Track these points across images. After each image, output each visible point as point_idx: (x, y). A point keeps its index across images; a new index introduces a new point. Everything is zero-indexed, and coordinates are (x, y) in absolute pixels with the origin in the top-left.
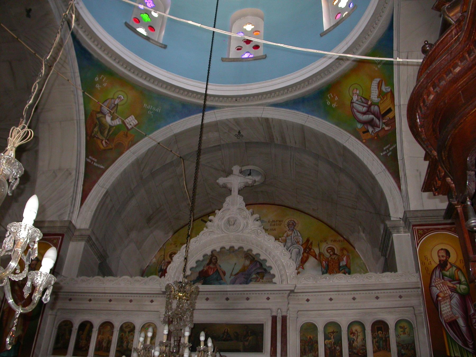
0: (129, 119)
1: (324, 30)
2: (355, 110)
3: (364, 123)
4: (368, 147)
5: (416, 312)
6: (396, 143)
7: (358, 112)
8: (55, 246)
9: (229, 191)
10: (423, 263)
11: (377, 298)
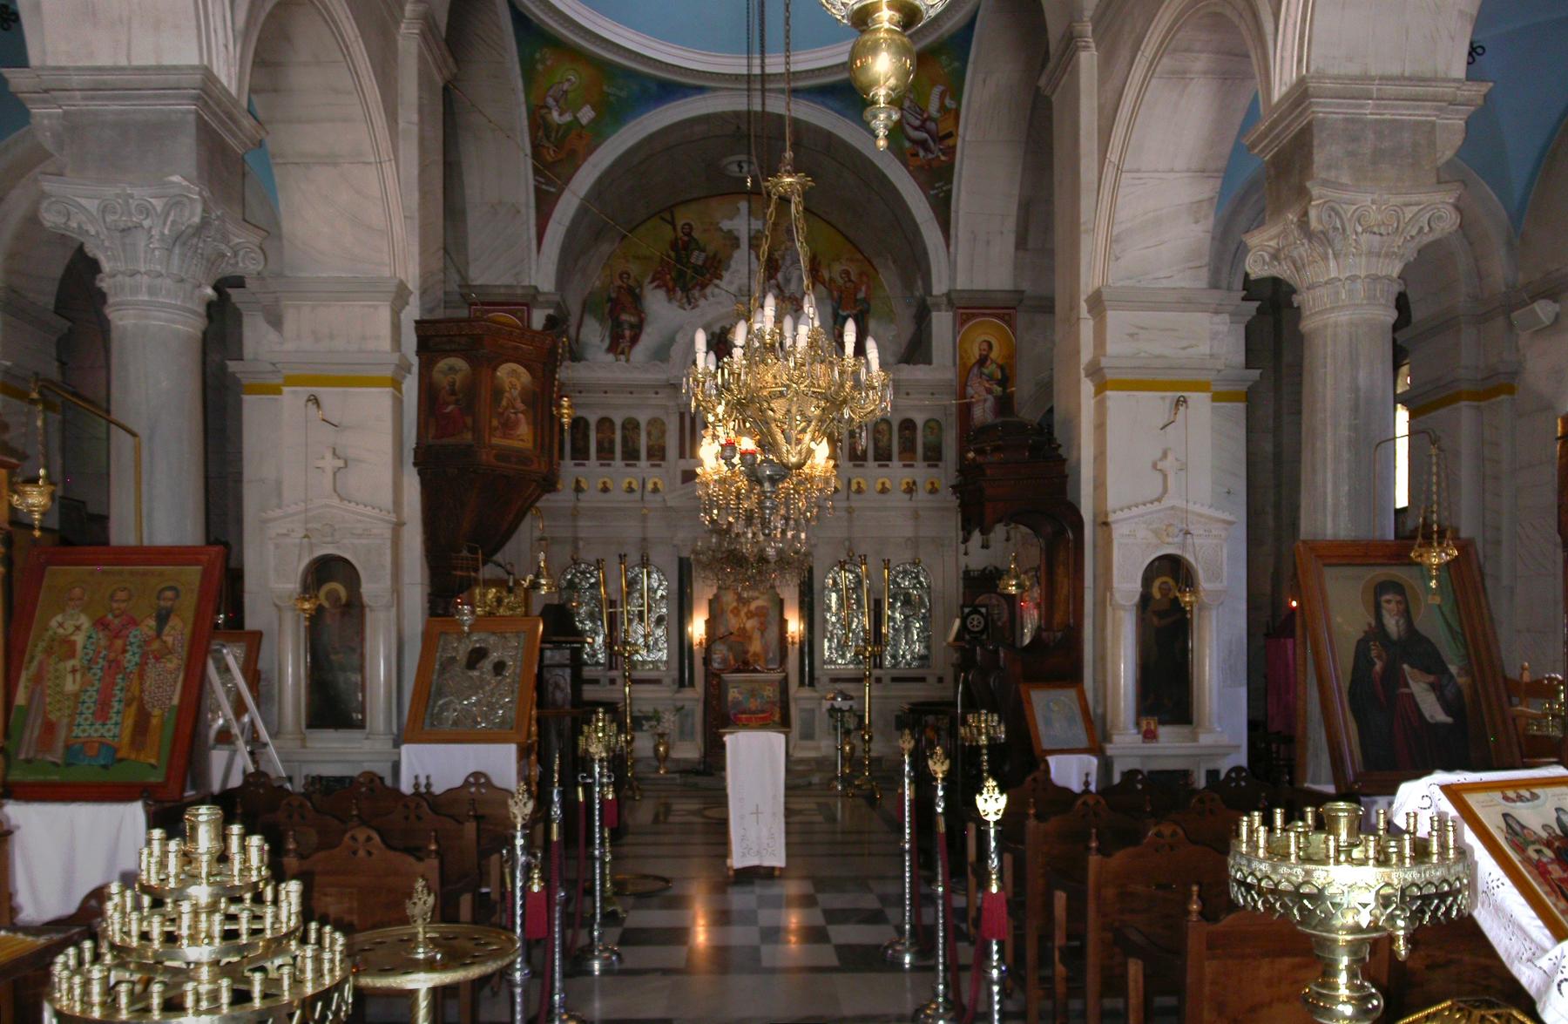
4: (915, 178)
8: (537, 332)
10: (961, 358)
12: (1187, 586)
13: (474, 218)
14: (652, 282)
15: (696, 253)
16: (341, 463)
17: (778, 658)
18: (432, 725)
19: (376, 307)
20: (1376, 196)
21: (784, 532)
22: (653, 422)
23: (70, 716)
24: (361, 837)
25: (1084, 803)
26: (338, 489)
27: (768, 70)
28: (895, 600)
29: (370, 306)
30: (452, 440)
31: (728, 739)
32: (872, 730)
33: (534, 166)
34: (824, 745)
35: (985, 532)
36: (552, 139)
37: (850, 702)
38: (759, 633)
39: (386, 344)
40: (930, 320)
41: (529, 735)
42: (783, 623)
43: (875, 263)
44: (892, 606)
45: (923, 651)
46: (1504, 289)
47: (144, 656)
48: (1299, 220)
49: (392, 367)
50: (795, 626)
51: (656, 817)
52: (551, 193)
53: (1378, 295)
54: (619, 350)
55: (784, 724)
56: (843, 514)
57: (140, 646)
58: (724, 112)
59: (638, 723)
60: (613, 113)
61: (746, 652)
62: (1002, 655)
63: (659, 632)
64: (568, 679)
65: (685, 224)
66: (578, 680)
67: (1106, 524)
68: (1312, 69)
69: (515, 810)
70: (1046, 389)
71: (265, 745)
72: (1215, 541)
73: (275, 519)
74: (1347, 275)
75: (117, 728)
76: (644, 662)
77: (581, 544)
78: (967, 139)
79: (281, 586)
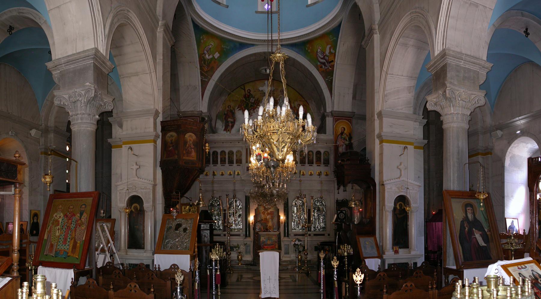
0: (216, 54)
1: (309, 4)
2: (318, 56)
3: (321, 63)
6: (333, 77)
7: (319, 57)
9: (264, 94)
10: (335, 132)
12: (407, 205)
13: (182, 91)
14: (238, 108)
15: (252, 99)
17: (277, 228)
18: (164, 248)
19: (149, 118)
20: (464, 90)
21: (279, 185)
22: (238, 152)
23: (57, 242)
24: (133, 286)
25: (380, 275)
26: (137, 175)
27: (273, 38)
28: (315, 210)
29: (147, 118)
30: (171, 158)
31: (260, 254)
32: (308, 251)
33: (200, 71)
34: (292, 256)
35: (345, 186)
36: (206, 64)
37: (301, 242)
38: (271, 220)
39: (152, 129)
40: (326, 119)
41: (194, 252)
42: (279, 217)
43: (308, 102)
44: (314, 211)
45: (323, 226)
46: (489, 126)
47: (76, 225)
48: (443, 94)
49: (154, 136)
50: (282, 217)
51: (238, 279)
52: (206, 81)
53: (464, 120)
54: (228, 129)
55: (279, 249)
56: (298, 182)
57: (75, 222)
58: (260, 52)
59: (232, 248)
60: (225, 54)
61: (267, 226)
62: (351, 226)
63: (239, 219)
64: (209, 234)
65: (248, 90)
66: (212, 235)
67: (383, 185)
68: (447, 47)
69: (177, 278)
70: (363, 142)
71: (115, 253)
72: (415, 192)
73: (119, 185)
74: (456, 112)
75: (68, 247)
76: (235, 229)
77: (215, 192)
78: (338, 63)
79: (121, 205)
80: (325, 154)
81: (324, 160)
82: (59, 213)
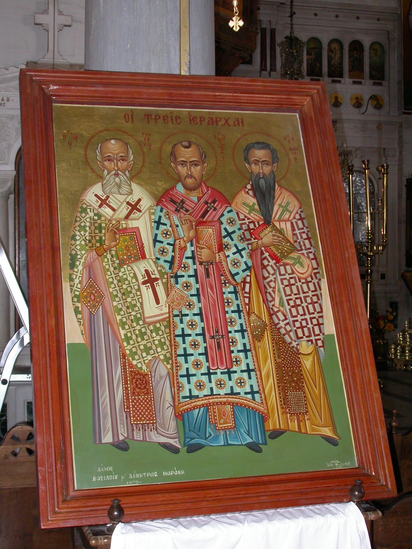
5: (390, 37)
11: (358, 18)
16: (40, 19)
23: (167, 359)
80: (374, 50)
81: (370, 67)
82: (119, 186)
